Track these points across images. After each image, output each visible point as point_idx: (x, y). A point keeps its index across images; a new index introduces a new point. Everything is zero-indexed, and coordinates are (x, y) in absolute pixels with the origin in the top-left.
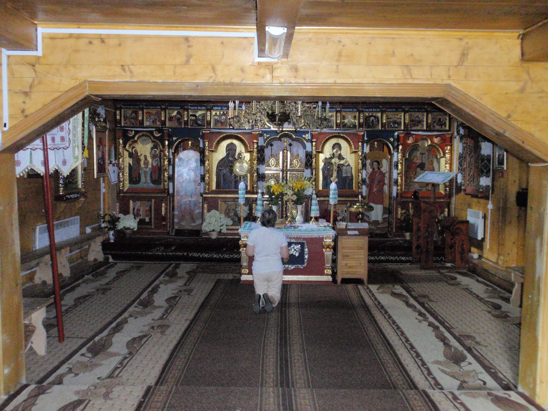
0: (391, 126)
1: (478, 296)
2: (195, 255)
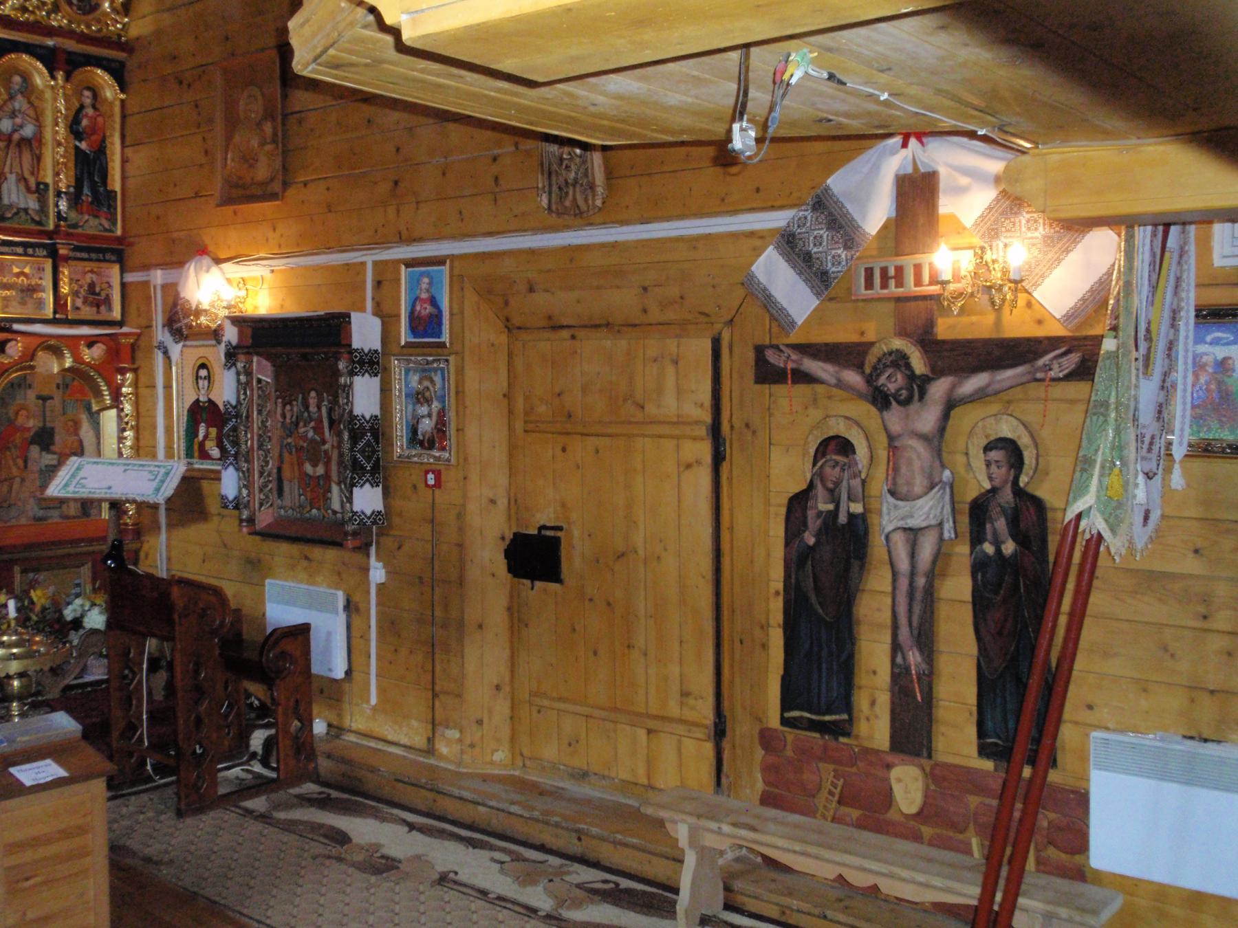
1: (484, 893)
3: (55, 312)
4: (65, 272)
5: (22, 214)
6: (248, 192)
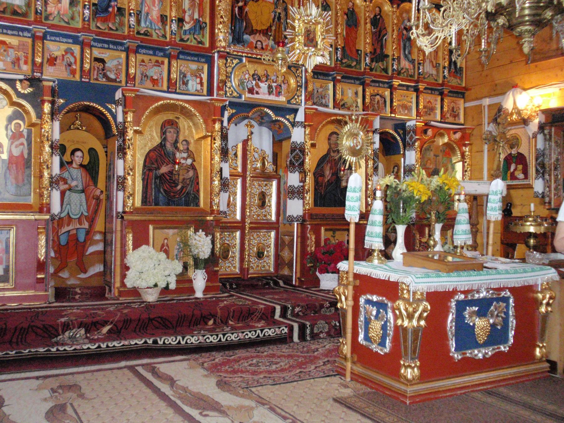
2: (171, 341)
3: (441, 119)
4: (446, 101)
5: (431, 76)
6: (546, 56)
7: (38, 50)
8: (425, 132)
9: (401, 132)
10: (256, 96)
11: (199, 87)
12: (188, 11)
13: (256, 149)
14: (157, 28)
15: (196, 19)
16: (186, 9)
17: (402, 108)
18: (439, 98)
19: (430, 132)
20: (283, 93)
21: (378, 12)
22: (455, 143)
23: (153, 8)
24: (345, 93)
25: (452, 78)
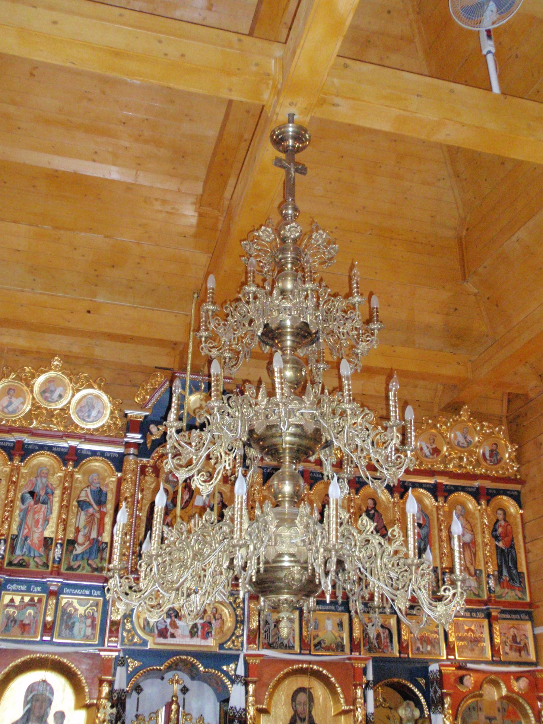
0: (418, 649)
3: (493, 656)
7: (72, 510)
8: (461, 680)
9: (423, 681)
10: (170, 640)
11: (89, 631)
12: (83, 530)
13: (189, 717)
14: (37, 554)
15: (94, 539)
16: (81, 527)
17: (421, 644)
18: (486, 623)
19: (470, 681)
20: (213, 633)
21: (372, 506)
22: (522, 696)
23: (35, 529)
24: (321, 626)
25: (506, 590)
